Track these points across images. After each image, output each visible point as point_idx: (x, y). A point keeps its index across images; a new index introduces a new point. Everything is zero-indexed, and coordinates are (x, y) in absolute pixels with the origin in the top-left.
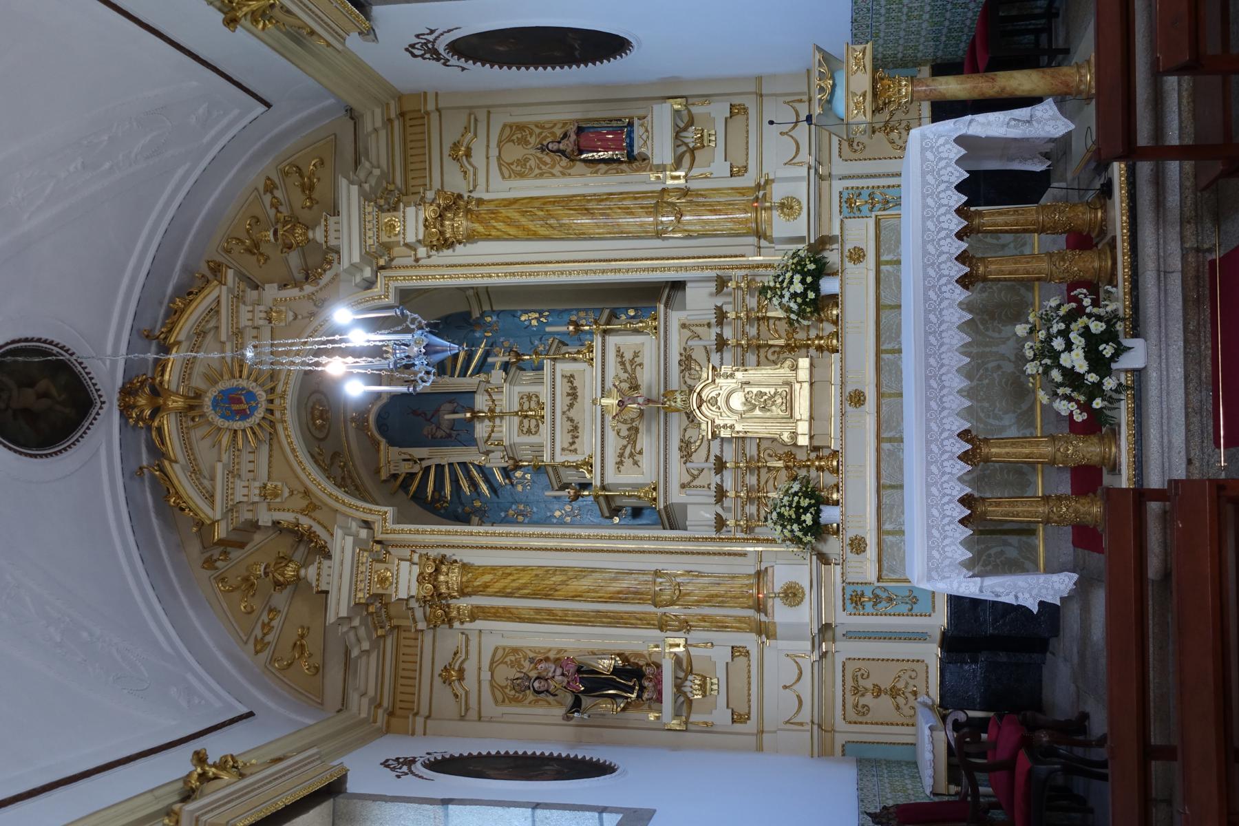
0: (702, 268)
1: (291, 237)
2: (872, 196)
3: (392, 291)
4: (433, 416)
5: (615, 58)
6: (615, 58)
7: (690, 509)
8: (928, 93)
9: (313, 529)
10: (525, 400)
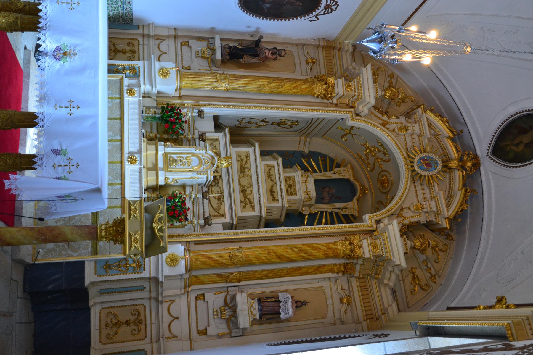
4: (332, 197)
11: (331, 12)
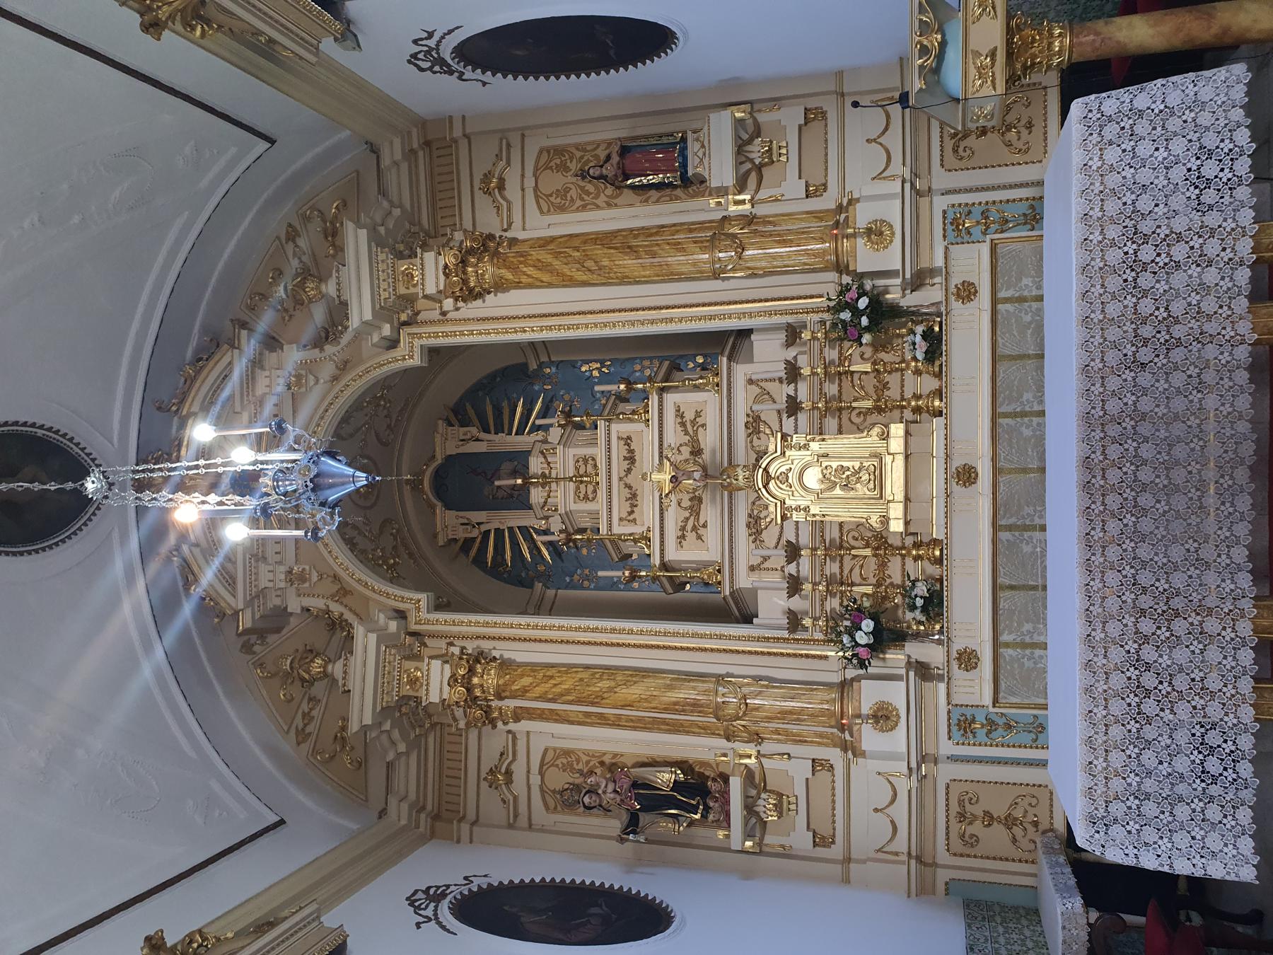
0: (770, 313)
1: (302, 293)
2: (985, 214)
3: (417, 351)
5: (659, 57)
6: (659, 57)
7: (761, 595)
8: (1097, 44)
10: (581, 463)
11: (429, 888)
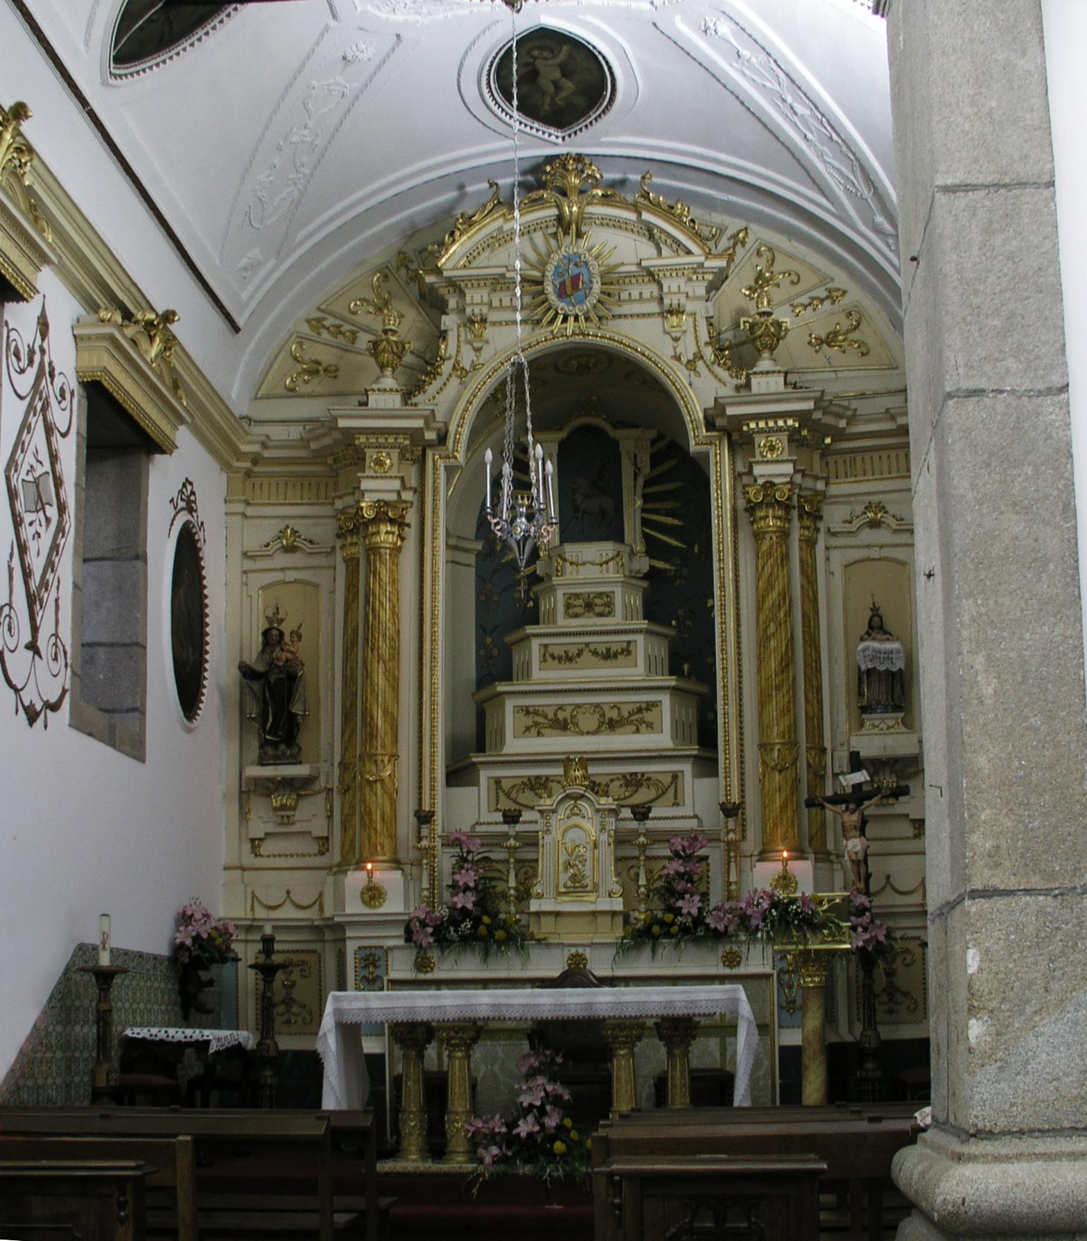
3: (704, 448)
7: (475, 789)
9: (438, 377)
